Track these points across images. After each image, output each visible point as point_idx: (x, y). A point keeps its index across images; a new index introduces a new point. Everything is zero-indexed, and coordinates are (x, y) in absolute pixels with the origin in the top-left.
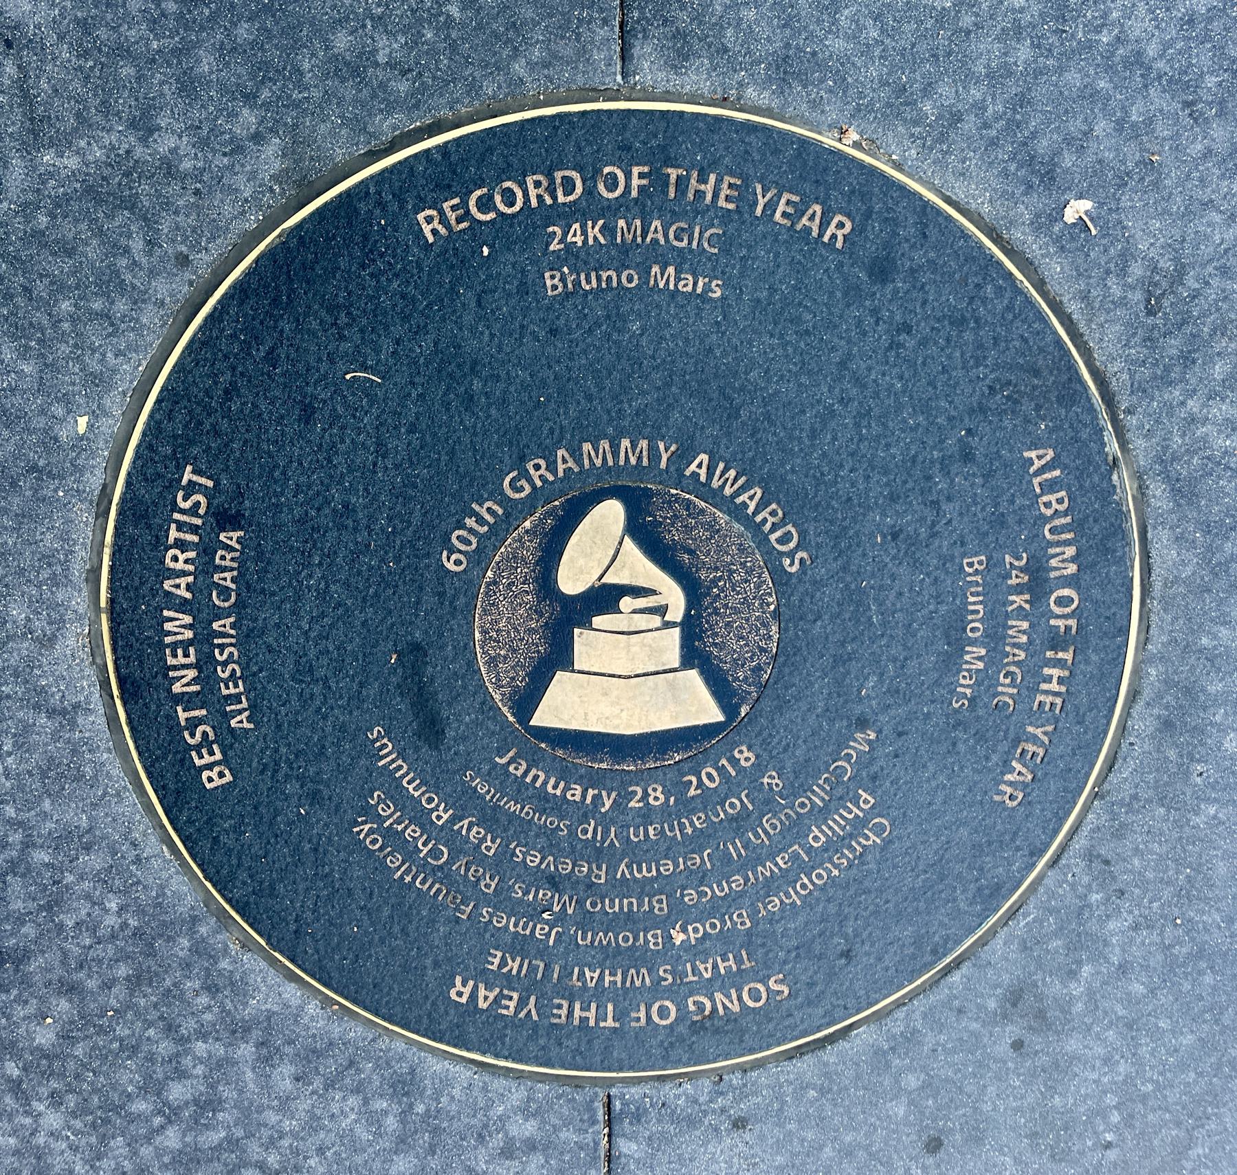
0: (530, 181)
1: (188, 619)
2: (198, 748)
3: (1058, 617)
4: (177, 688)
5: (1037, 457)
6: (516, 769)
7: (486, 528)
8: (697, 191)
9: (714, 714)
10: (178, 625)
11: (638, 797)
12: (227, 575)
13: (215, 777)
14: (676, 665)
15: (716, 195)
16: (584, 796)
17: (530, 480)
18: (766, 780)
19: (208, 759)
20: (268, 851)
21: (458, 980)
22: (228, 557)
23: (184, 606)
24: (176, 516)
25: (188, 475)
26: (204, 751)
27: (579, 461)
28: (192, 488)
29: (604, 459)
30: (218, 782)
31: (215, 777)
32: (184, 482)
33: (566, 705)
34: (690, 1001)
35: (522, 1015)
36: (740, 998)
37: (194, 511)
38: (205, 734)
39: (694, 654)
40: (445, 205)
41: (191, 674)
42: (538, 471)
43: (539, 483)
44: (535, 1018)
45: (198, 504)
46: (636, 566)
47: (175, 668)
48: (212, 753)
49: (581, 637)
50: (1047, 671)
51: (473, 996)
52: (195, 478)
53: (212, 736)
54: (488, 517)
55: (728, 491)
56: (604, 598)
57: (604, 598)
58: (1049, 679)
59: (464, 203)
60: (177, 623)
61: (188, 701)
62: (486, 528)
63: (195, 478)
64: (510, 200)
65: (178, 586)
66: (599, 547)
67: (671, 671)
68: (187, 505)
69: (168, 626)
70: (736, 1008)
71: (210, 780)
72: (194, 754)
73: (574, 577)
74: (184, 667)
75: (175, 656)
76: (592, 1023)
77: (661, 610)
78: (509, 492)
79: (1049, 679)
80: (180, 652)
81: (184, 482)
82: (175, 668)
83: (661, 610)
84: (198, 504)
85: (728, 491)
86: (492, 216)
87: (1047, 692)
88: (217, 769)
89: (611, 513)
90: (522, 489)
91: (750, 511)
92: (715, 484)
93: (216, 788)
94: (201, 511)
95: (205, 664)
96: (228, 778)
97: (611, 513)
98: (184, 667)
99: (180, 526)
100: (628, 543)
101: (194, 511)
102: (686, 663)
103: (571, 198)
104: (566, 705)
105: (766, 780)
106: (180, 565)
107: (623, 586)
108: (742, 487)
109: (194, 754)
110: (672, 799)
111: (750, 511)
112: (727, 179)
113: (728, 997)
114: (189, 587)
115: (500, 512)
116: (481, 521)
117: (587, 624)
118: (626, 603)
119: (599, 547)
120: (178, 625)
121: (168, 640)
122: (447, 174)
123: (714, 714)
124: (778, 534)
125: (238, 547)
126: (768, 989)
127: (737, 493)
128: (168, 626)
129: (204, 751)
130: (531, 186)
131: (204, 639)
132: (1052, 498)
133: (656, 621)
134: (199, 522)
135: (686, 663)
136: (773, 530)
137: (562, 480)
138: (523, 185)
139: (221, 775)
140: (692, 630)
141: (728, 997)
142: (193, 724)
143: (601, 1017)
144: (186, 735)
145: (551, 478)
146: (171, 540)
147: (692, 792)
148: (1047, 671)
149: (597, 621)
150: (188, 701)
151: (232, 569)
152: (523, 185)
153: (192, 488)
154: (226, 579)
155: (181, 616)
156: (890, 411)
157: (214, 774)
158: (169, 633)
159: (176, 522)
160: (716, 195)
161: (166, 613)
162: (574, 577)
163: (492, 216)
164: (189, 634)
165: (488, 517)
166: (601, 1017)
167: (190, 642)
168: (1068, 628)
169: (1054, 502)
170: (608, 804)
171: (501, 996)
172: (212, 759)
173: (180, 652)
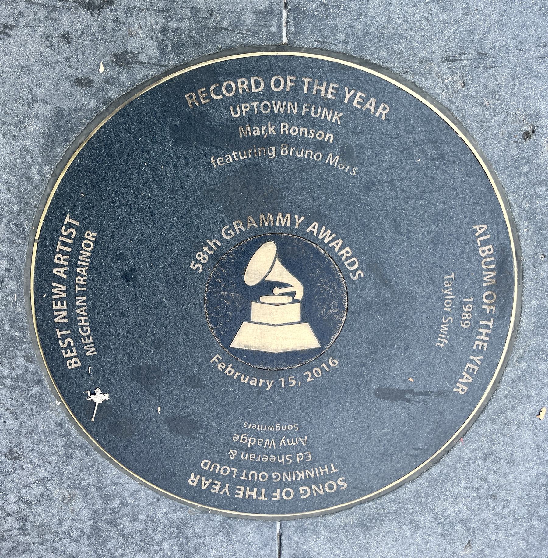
1: (63, 288)
2: (65, 349)
4: (56, 320)
7: (212, 252)
8: (486, 336)
10: (59, 290)
11: (310, 376)
13: (73, 363)
14: (298, 319)
15: (327, 91)
16: (258, 383)
18: (231, 451)
21: (193, 475)
22: (82, 279)
23: (60, 280)
24: (61, 238)
25: (68, 219)
26: (69, 351)
30: (74, 366)
31: (73, 363)
32: (59, 337)
33: (247, 337)
34: (301, 489)
35: (222, 493)
37: (69, 236)
38: (69, 343)
40: (199, 91)
41: (65, 313)
43: (238, 232)
44: (228, 494)
46: (281, 274)
48: (72, 352)
49: (255, 305)
52: (63, 333)
53: (72, 344)
54: (214, 247)
55: (326, 241)
56: (267, 287)
57: (267, 287)
58: (481, 334)
61: (62, 327)
62: (212, 252)
63: (63, 333)
65: (60, 272)
66: (264, 263)
68: (66, 234)
69: (54, 291)
71: (70, 364)
72: (63, 351)
73: (254, 273)
75: (57, 304)
76: (254, 498)
77: (292, 294)
78: (224, 235)
80: (59, 303)
81: (59, 337)
84: (71, 233)
85: (326, 241)
86: (220, 97)
88: (74, 359)
89: (267, 252)
90: (303, 490)
91: (336, 250)
92: (320, 237)
94: (73, 237)
95: (72, 308)
97: (267, 252)
99: (64, 244)
100: (277, 262)
101: (69, 236)
102: (304, 320)
104: (247, 337)
105: (231, 451)
107: (277, 282)
108: (333, 238)
109: (63, 351)
111: (336, 250)
112: (331, 85)
116: (210, 248)
117: (258, 300)
118: (277, 291)
119: (264, 263)
120: (59, 290)
125: (86, 274)
126: (337, 484)
127: (330, 242)
129: (69, 351)
130: (239, 83)
131: (71, 297)
132: (486, 248)
133: (290, 299)
134: (71, 241)
135: (304, 320)
136: (346, 260)
138: (236, 83)
139: (76, 363)
141: (311, 472)
143: (259, 494)
144: (60, 342)
145: (86, 278)
147: (309, 380)
149: (263, 299)
150: (62, 327)
152: (236, 83)
154: (82, 271)
155: (60, 286)
157: (72, 362)
160: (327, 91)
164: (64, 295)
165: (214, 247)
166: (259, 494)
167: (64, 298)
170: (269, 386)
171: (213, 483)
172: (72, 355)
173: (59, 303)
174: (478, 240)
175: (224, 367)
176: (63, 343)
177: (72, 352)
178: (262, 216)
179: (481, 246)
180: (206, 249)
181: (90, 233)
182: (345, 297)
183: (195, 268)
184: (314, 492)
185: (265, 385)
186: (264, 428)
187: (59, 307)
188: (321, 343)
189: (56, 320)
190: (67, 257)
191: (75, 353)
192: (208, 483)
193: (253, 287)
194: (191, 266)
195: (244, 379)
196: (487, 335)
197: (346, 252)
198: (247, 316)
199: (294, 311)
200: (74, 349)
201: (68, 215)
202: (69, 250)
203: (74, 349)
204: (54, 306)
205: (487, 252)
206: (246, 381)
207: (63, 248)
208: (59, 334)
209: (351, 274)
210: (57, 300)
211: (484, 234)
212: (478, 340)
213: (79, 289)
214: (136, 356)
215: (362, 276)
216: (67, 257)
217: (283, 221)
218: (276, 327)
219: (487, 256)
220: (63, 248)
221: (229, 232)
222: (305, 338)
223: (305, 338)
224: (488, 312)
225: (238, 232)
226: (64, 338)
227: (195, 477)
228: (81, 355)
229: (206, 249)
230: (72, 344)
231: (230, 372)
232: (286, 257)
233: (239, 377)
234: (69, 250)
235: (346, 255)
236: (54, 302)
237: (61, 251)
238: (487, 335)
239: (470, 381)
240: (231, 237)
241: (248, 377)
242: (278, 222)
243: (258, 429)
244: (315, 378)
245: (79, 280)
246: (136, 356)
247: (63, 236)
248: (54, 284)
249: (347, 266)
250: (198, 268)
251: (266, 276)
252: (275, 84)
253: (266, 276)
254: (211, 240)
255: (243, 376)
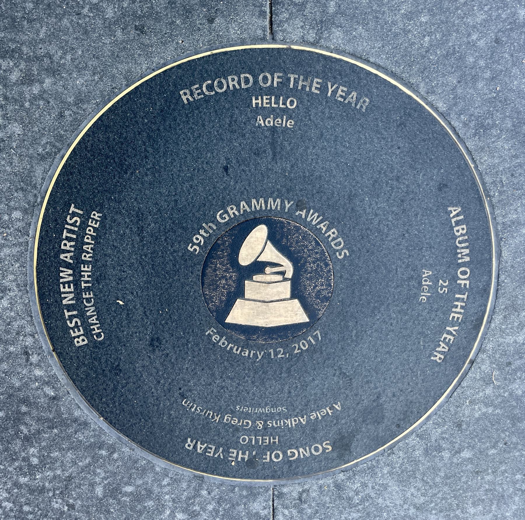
0: (230, 78)
1: (70, 272)
2: (72, 328)
3: (462, 280)
4: (64, 302)
5: (454, 211)
6: (244, 354)
9: (304, 318)
11: (281, 353)
12: (69, 255)
14: (288, 296)
17: (229, 216)
19: (77, 334)
20: (98, 375)
21: (189, 440)
23: (68, 266)
24: (66, 226)
25: (72, 209)
26: (76, 330)
27: (250, 207)
28: (74, 214)
29: (261, 206)
30: (81, 343)
33: (240, 314)
34: (289, 452)
35: (216, 456)
36: (299, 452)
38: (76, 322)
39: (296, 293)
41: (71, 296)
42: (232, 211)
45: (76, 221)
46: (272, 254)
47: (65, 293)
48: (79, 331)
50: (456, 303)
51: (195, 447)
53: (79, 324)
55: (314, 223)
56: (258, 267)
57: (258, 267)
58: (456, 306)
59: (201, 88)
60: (65, 273)
61: (69, 308)
64: (221, 86)
66: (256, 245)
67: (284, 300)
70: (301, 450)
71: (78, 342)
73: (245, 257)
74: (67, 293)
75: (64, 288)
77: (283, 273)
79: (456, 306)
80: (66, 285)
82: (65, 293)
83: (283, 273)
84: (76, 221)
85: (314, 223)
86: (214, 93)
87: (456, 312)
88: (81, 338)
89: (261, 232)
90: (291, 452)
92: (309, 219)
93: (461, 225)
96: (86, 342)
97: (261, 232)
98: (67, 293)
99: (69, 231)
102: (293, 296)
103: (248, 86)
104: (240, 314)
106: (68, 248)
110: (288, 354)
111: (72, 254)
113: (306, 450)
114: (71, 258)
115: (215, 228)
117: (250, 278)
118: (268, 270)
119: (256, 245)
120: (66, 275)
121: (61, 280)
122: (191, 73)
123: (304, 318)
124: (334, 242)
125: (92, 252)
128: (61, 274)
129: (76, 330)
130: (230, 80)
133: (279, 278)
135: (293, 296)
137: (242, 215)
139: (458, 231)
140: (295, 282)
141: (306, 450)
142: (71, 318)
144: (68, 322)
145: (91, 255)
146: (64, 237)
148: (456, 303)
149: (255, 278)
150: (69, 308)
151: (71, 251)
153: (74, 214)
156: (382, 186)
158: (62, 278)
159: (67, 229)
161: (61, 269)
162: (245, 257)
163: (213, 93)
164: (71, 278)
168: (465, 284)
169: (460, 230)
173: (66, 285)
174: (453, 221)
175: (218, 339)
176: (71, 323)
177: (79, 331)
178: (254, 201)
179: (91, 298)
180: (202, 232)
181: (96, 213)
182: (331, 275)
183: (192, 250)
184: (301, 454)
185: (256, 355)
186: (255, 410)
187: (67, 289)
188: (309, 317)
189: (64, 302)
190: (73, 243)
191: (82, 332)
192: (203, 447)
193: (246, 267)
194: (189, 248)
195: (237, 350)
196: (462, 307)
197: (333, 233)
198: (240, 293)
199: (285, 289)
200: (81, 328)
201: (73, 205)
202: (74, 236)
203: (81, 328)
204: (62, 290)
205: (461, 231)
206: (238, 352)
207: (69, 235)
208: (67, 314)
209: (338, 253)
210: (64, 283)
211: (457, 215)
212: (453, 312)
213: (85, 285)
214: (138, 324)
215: (348, 254)
216: (73, 243)
217: (274, 204)
218: (267, 303)
219: (462, 235)
220: (69, 235)
221: (223, 216)
222: (294, 314)
223: (294, 314)
224: (463, 286)
225: (232, 216)
226: (71, 318)
227: (192, 441)
228: (88, 333)
229: (202, 232)
230: (79, 324)
231: (223, 344)
232: (273, 238)
233: (231, 348)
234: (74, 236)
235: (332, 236)
236: (61, 285)
237: (67, 238)
238: (462, 307)
239: (446, 350)
240: (226, 220)
241: (240, 349)
242: (269, 206)
243: (250, 412)
244: (302, 349)
245: (94, 215)
246: (138, 324)
247: (68, 224)
248: (61, 269)
249: (333, 246)
250: (195, 250)
251: (258, 257)
252: (267, 80)
253: (258, 257)
254: (207, 224)
255: (236, 347)
